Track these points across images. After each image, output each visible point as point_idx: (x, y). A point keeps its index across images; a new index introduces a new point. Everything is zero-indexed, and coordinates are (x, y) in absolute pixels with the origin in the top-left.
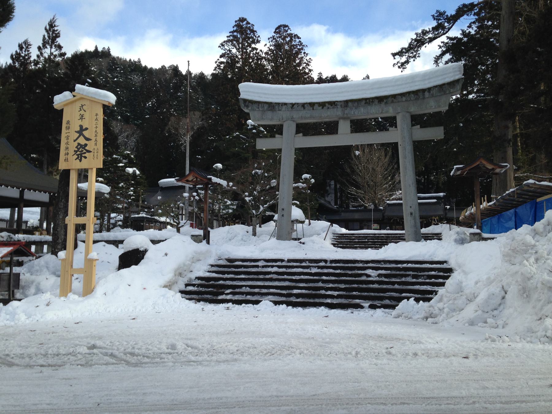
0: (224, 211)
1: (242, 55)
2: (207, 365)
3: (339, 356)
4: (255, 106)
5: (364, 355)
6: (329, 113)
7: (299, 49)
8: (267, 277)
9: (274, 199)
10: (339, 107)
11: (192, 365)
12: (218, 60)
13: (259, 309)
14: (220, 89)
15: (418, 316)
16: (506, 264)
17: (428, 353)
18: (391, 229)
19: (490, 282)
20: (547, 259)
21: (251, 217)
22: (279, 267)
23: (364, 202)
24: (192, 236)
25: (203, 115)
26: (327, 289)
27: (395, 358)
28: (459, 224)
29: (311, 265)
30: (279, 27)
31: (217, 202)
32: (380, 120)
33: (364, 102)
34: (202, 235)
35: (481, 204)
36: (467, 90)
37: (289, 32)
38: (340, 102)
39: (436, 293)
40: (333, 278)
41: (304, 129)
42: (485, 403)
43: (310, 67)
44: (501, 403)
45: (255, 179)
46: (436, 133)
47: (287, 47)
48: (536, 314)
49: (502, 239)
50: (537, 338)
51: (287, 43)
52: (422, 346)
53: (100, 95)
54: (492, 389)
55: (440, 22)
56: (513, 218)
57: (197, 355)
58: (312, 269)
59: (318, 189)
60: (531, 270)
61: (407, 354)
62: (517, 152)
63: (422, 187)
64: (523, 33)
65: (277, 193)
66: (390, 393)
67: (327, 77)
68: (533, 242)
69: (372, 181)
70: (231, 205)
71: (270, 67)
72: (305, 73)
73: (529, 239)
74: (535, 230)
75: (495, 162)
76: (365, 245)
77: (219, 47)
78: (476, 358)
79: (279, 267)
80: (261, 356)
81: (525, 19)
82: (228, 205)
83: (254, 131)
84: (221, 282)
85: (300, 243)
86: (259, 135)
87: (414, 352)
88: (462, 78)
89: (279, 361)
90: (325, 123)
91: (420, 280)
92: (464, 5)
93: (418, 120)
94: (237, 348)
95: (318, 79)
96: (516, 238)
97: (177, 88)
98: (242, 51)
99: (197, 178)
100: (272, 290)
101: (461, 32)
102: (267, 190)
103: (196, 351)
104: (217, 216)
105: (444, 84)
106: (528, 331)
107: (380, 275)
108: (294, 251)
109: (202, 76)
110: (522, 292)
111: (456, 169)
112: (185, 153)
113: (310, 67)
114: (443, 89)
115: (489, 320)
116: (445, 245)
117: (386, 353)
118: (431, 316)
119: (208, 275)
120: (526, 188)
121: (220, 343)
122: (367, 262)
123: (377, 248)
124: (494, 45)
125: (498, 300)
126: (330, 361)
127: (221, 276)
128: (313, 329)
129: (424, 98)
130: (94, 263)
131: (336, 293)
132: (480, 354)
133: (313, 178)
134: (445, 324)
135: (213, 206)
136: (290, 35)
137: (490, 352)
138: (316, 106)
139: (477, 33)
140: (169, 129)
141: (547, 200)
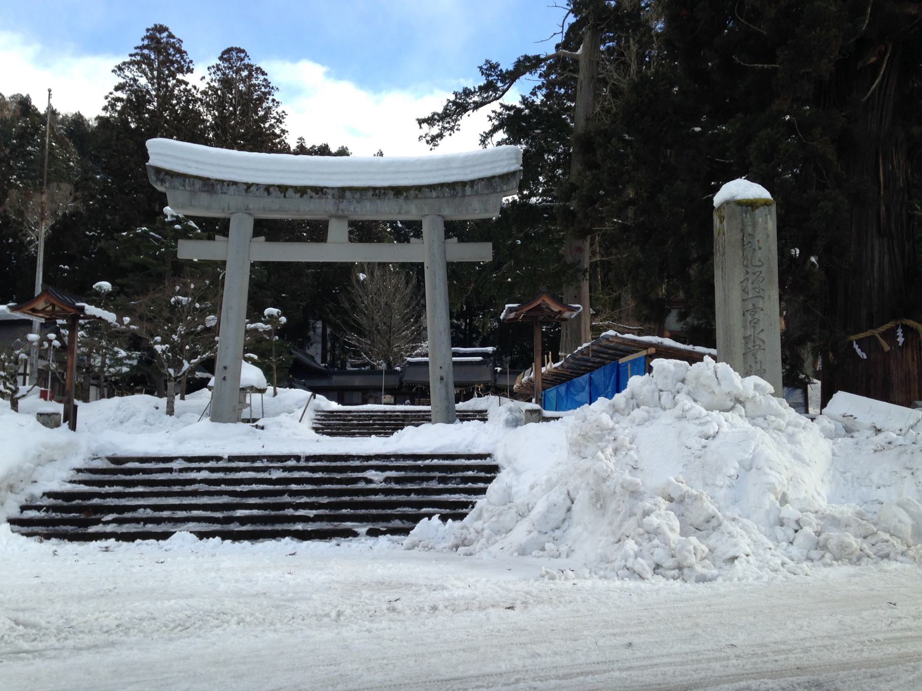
0: (111, 370)
1: (158, 90)
2: (55, 657)
3: (307, 622)
4: (177, 182)
5: (351, 616)
7: (264, 93)
8: (188, 488)
9: (211, 348)
10: (330, 197)
11: (22, 659)
12: (111, 93)
13: (168, 547)
14: (112, 148)
15: (444, 545)
16: (574, 457)
17: (453, 604)
18: (412, 403)
19: (551, 485)
20: (629, 450)
21: (166, 381)
22: (212, 470)
23: (370, 358)
24: (40, 415)
25: (76, 190)
26: (298, 506)
27: (401, 617)
28: (514, 396)
29: (271, 465)
30: (229, 51)
31: (98, 352)
32: (400, 225)
33: (371, 193)
34: (62, 412)
35: (543, 365)
36: (528, 188)
37: (246, 61)
38: (333, 188)
39: (473, 504)
40: (309, 487)
41: (268, 229)
42: (534, 679)
43: (282, 126)
44: (558, 677)
45: (175, 313)
46: (481, 252)
47: (242, 87)
48: (614, 533)
49: (570, 419)
50: (613, 570)
51: (243, 80)
52: (446, 594)
54: (546, 655)
55: (491, 78)
56: (587, 388)
57: (34, 640)
58: (273, 472)
59: (294, 333)
60: (607, 466)
61: (422, 609)
62: (596, 289)
63: (460, 337)
64: (608, 111)
65: (217, 338)
66: (388, 678)
67: (314, 146)
68: (611, 424)
69: (385, 324)
70: (126, 359)
71: (210, 118)
72: (274, 134)
73: (606, 419)
74: (614, 406)
75: (565, 302)
76: (368, 429)
77: (114, 71)
78: (526, 607)
79: (212, 470)
80: (164, 632)
81: (611, 91)
82: (121, 359)
83: (177, 226)
84: (96, 501)
85: (257, 427)
86: (186, 233)
87: (432, 604)
89: (198, 640)
90: (309, 223)
91: (450, 486)
92: (526, 58)
93: (455, 230)
94: (117, 622)
95: (298, 147)
96: (588, 418)
97: (26, 136)
98: (159, 84)
99: (54, 306)
100: (195, 513)
101: (520, 99)
102: (198, 334)
103: (34, 631)
104: (97, 378)
106: (602, 561)
107: (387, 480)
108: (242, 442)
109: (78, 120)
110: (594, 500)
111: (508, 310)
112: (35, 259)
113: (282, 126)
114: (494, 183)
116: (484, 429)
117: (388, 609)
118: (464, 542)
119: (69, 487)
120: (604, 343)
121: (83, 615)
122: (368, 458)
123: (387, 434)
124: (568, 125)
125: (561, 514)
126: (292, 632)
127: (95, 489)
128: (266, 577)
129: (464, 196)
131: (312, 513)
132: (531, 601)
133: (284, 314)
134: (484, 555)
135: (89, 360)
136: (249, 67)
137: (545, 596)
138: (290, 193)
139: (543, 103)
140: (5, 211)
141: (633, 362)
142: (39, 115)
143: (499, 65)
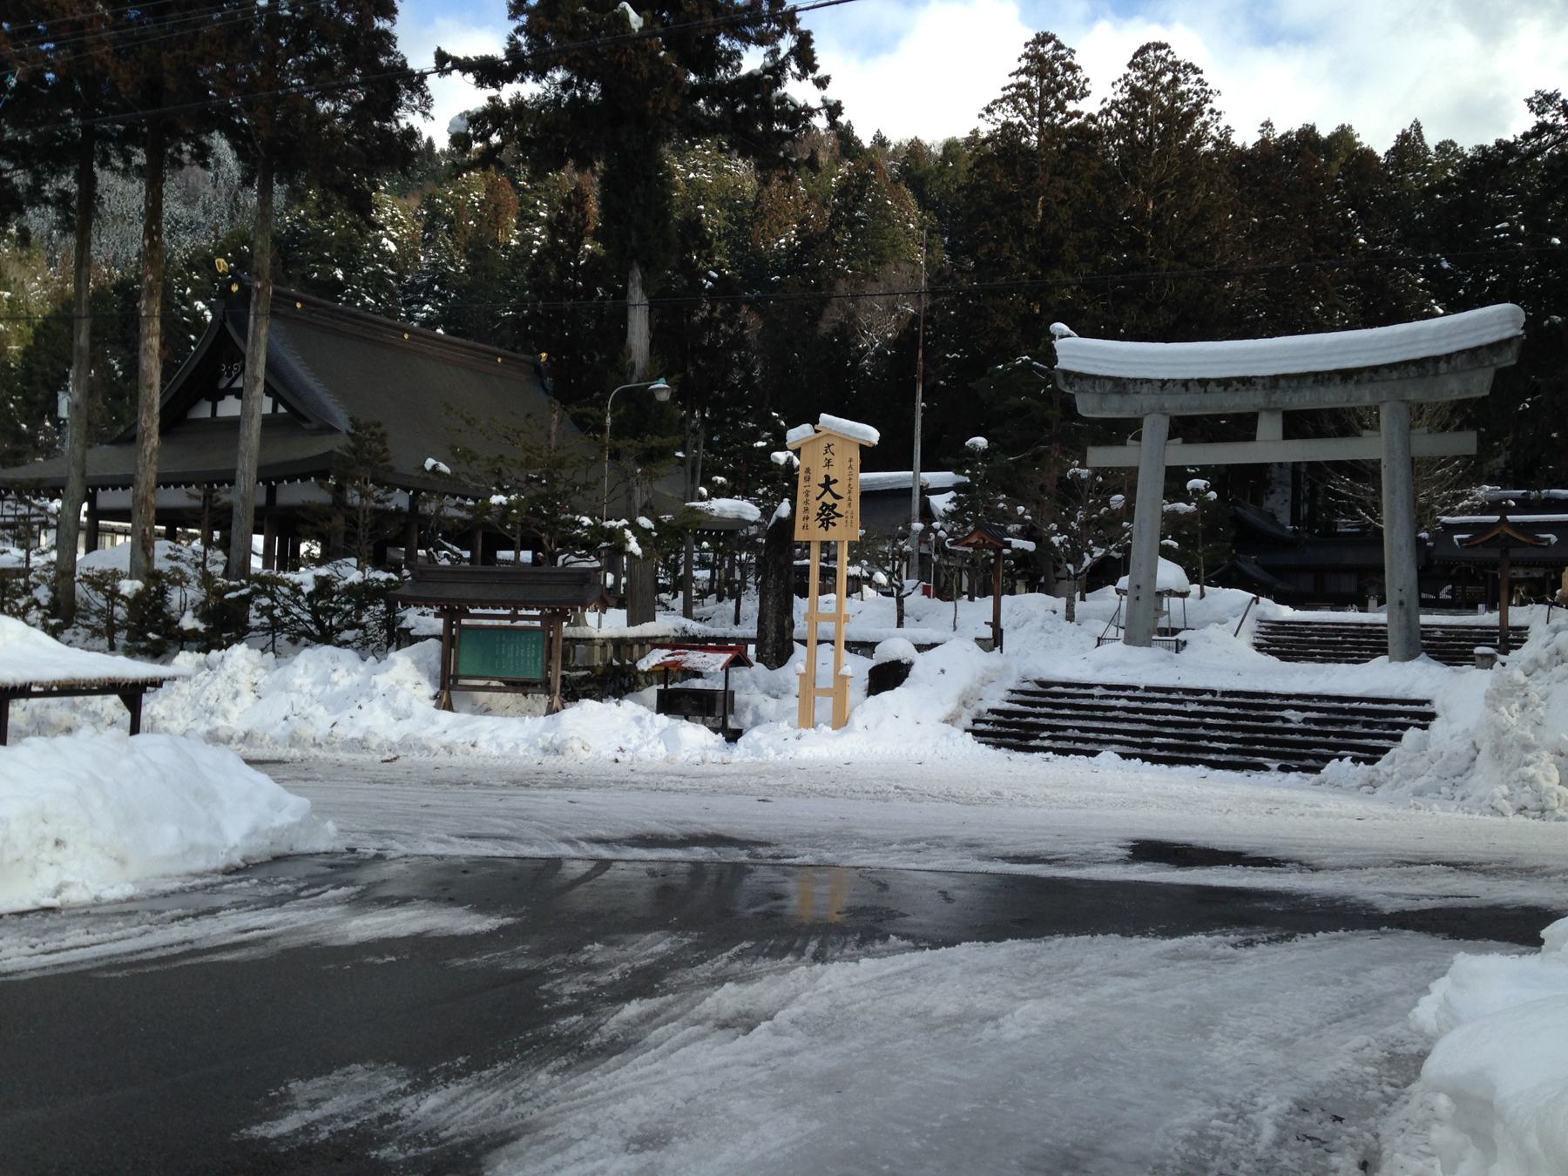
4: (1087, 385)
6: (1237, 400)
8: (1109, 714)
22: (1130, 699)
26: (1211, 739)
30: (1143, 50)
33: (1310, 380)
51: (1165, 89)
53: (857, 431)
67: (1289, 133)
79: (1130, 699)
84: (1030, 719)
88: (1518, 337)
98: (1041, 123)
105: (1480, 347)
107: (1306, 720)
115: (1443, 789)
119: (1007, 706)
122: (1289, 697)
125: (1464, 763)
127: (1029, 709)
129: (1437, 374)
130: (849, 682)
131: (1225, 746)
142: (862, 150)
143: (1558, 96)
